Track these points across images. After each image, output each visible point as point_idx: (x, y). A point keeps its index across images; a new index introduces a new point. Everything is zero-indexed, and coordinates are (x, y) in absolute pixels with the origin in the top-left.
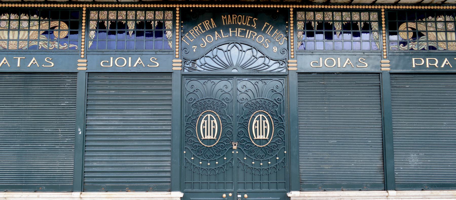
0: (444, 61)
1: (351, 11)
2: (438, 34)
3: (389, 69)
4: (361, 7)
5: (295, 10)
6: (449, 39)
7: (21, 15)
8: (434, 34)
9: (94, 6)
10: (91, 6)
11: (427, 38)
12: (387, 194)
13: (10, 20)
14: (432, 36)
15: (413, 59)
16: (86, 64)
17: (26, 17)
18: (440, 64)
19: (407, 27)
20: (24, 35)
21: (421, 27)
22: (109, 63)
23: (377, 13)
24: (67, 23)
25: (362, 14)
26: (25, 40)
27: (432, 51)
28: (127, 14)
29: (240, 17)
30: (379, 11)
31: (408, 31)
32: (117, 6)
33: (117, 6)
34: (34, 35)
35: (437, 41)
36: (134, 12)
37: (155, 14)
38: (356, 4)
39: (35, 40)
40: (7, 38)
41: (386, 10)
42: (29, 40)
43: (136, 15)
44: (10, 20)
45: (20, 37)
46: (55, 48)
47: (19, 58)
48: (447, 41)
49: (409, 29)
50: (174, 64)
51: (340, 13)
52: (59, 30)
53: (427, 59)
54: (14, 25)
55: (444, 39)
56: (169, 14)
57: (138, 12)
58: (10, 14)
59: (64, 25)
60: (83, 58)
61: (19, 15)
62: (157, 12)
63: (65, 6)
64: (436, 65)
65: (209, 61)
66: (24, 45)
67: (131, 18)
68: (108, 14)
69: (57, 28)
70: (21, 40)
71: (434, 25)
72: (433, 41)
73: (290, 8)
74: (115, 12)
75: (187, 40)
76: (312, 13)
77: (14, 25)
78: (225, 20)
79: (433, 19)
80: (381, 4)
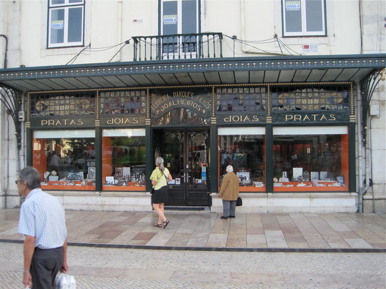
0: (305, 116)
3: (215, 123)
4: (255, 84)
5: (216, 88)
6: (309, 103)
7: (314, 89)
9: (103, 89)
10: (101, 89)
13: (60, 99)
14: (52, 108)
15: (286, 116)
17: (317, 91)
18: (55, 123)
19: (40, 103)
21: (47, 103)
23: (265, 88)
28: (120, 94)
29: (184, 93)
30: (146, 90)
31: (40, 106)
32: (115, 89)
33: (115, 89)
34: (72, 107)
35: (55, 111)
37: (135, 93)
38: (281, 82)
39: (73, 110)
40: (59, 109)
42: (320, 104)
43: (125, 94)
44: (60, 99)
45: (66, 108)
46: (83, 114)
47: (65, 120)
49: (41, 105)
50: (146, 122)
51: (242, 89)
52: (85, 105)
53: (295, 116)
56: (144, 93)
57: (126, 92)
58: (60, 96)
60: (98, 119)
61: (313, 89)
64: (300, 119)
66: (67, 113)
72: (53, 111)
73: (212, 86)
74: (114, 93)
76: (226, 89)
78: (175, 95)
79: (300, 91)
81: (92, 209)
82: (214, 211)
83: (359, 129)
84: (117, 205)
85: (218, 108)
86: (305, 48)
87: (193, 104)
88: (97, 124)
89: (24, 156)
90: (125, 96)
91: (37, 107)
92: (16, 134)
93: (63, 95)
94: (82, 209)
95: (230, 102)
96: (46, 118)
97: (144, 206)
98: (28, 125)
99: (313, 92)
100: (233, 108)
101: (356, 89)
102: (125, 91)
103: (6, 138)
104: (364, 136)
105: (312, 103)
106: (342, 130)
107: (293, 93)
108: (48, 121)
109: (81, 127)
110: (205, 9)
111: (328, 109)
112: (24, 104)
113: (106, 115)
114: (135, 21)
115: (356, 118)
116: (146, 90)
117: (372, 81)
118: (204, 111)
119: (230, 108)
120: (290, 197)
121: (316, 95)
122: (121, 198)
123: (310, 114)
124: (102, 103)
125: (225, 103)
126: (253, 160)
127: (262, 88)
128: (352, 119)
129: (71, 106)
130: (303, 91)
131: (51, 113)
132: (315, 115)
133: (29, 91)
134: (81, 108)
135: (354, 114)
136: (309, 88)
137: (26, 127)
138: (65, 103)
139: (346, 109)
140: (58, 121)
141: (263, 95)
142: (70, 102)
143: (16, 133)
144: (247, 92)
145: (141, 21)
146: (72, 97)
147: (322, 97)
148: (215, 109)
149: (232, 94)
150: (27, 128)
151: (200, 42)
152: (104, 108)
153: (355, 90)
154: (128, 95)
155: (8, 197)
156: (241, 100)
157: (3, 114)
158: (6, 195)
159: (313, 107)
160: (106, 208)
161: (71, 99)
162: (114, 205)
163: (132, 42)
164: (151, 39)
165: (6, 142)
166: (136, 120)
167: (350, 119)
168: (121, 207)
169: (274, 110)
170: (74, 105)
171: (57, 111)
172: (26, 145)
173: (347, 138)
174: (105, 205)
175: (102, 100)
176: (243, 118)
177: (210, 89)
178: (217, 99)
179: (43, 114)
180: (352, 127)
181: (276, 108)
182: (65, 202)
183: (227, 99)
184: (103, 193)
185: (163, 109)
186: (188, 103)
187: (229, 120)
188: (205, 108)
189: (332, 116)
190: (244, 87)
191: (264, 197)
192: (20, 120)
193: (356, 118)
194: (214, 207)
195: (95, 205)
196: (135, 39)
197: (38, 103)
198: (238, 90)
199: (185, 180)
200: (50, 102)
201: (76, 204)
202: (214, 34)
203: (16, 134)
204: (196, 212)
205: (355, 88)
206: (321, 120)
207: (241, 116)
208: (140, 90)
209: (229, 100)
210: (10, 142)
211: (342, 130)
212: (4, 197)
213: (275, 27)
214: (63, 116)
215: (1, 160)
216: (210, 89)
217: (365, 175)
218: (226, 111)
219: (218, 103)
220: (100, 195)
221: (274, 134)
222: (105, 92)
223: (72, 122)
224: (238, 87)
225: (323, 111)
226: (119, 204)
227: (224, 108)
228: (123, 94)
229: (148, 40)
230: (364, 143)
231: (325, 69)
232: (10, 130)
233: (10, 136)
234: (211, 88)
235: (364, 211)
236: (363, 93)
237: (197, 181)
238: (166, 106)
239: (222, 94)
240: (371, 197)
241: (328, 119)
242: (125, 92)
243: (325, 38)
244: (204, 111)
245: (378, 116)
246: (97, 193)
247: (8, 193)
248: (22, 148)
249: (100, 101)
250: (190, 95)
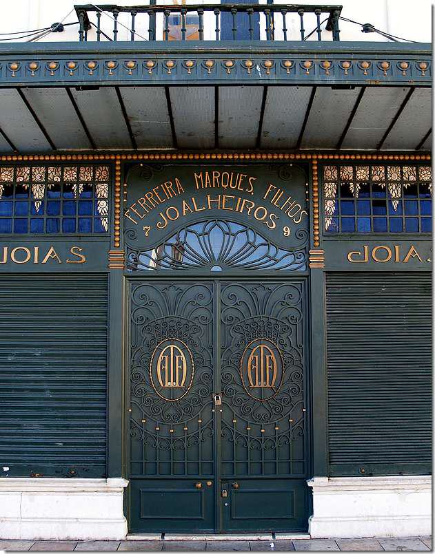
36: (43, 169)
43: (47, 174)
73: (312, 159)
74: (12, 169)
76: (350, 169)
152: (336, 212)
166: (79, 252)
176: (403, 254)
177: (305, 167)
190: (401, 164)
196: (81, 11)
198: (386, 170)
207: (36, 249)
216: (305, 167)
223: (49, 255)
242: (402, 169)
249: (322, 191)
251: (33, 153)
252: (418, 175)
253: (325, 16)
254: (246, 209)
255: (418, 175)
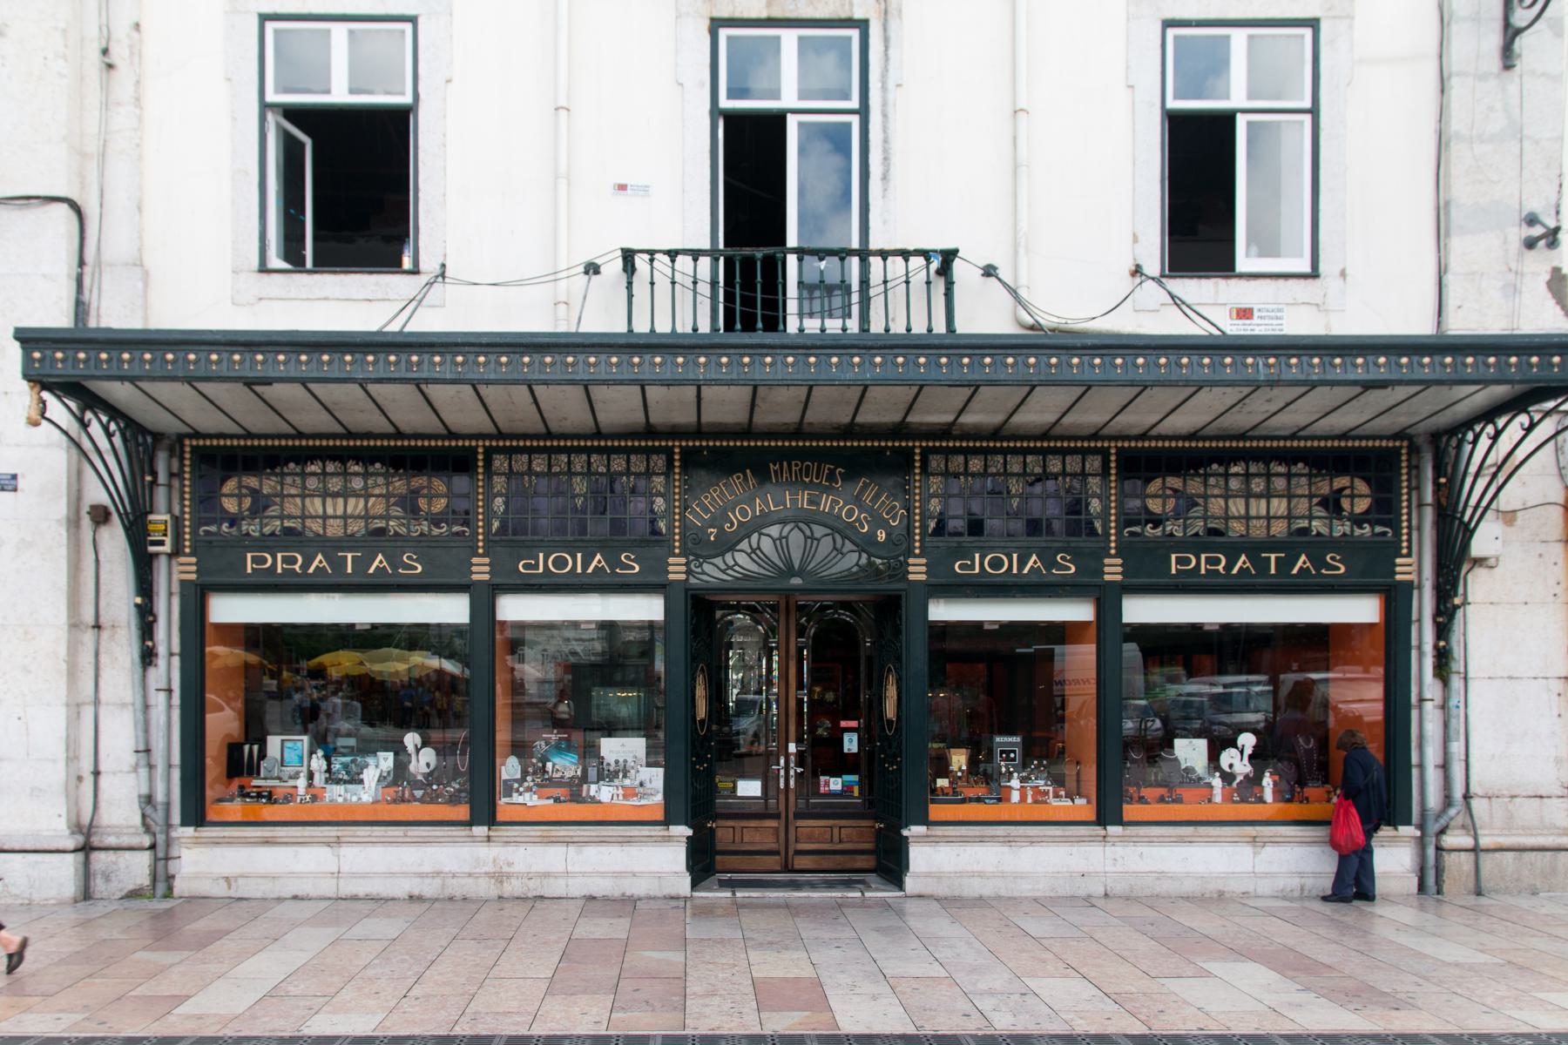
1: (549, 451)
2: (308, 500)
3: (487, 577)
8: (1222, 502)
11: (1206, 510)
12: (1103, 833)
13: (324, 473)
14: (1216, 506)
15: (1173, 556)
16: (684, 568)
17: (1282, 469)
18: (306, 566)
20: (356, 506)
22: (536, 566)
24: (1367, 480)
25: (1068, 459)
26: (359, 517)
27: (1212, 539)
28: (569, 462)
30: (1104, 453)
31: (1165, 497)
34: (1302, 506)
35: (304, 517)
36: (584, 457)
37: (628, 461)
39: (381, 517)
40: (321, 512)
41: (1120, 451)
42: (367, 517)
43: (589, 463)
44: (324, 473)
45: (349, 511)
46: (422, 534)
47: (349, 556)
48: (1247, 517)
49: (1169, 492)
52: (430, 498)
53: (1203, 556)
54: (1258, 485)
55: (1243, 512)
57: (594, 457)
59: (1361, 487)
60: (679, 556)
61: (1267, 465)
62: (633, 458)
63: (1336, 444)
64: (1220, 568)
65: (742, 559)
66: (356, 527)
67: (579, 469)
68: (530, 462)
69: (1348, 492)
70: (352, 517)
71: (1222, 483)
74: (545, 456)
75: (693, 512)
76: (961, 459)
77: (1258, 485)
79: (1221, 470)
80: (1110, 438)
81: (458, 893)
82: (916, 891)
83: (1424, 604)
84: (555, 875)
85: (932, 525)
86: (1239, 317)
87: (841, 509)
88: (481, 570)
89: (1421, 700)
90: (589, 473)
91: (224, 500)
92: (137, 605)
93: (341, 456)
94: (416, 892)
95: (976, 507)
96: (269, 543)
97: (659, 876)
98: (188, 568)
99: (345, 474)
100: (988, 523)
101: (1417, 467)
102: (589, 451)
103: (89, 618)
104: (1443, 630)
105: (340, 512)
106: (1362, 610)
107: (1199, 475)
108: (275, 559)
109: (633, 580)
110: (885, 159)
111: (1319, 534)
112: (169, 486)
113: (514, 538)
114: (622, 187)
115: (1416, 566)
116: (669, 452)
117: (1484, 442)
118: (881, 536)
119: (976, 527)
120: (1181, 840)
121: (357, 484)
122: (572, 849)
123: (1255, 549)
124: (499, 494)
125: (956, 508)
126: (408, 704)
127: (1090, 459)
128: (1404, 570)
129: (372, 500)
130: (1234, 469)
131: (287, 524)
132: (1273, 556)
133: (190, 436)
134: (413, 511)
135: (1409, 555)
136: (1256, 459)
137: (176, 577)
138: (346, 487)
139: (1384, 534)
140: (320, 557)
141: (658, 481)
142: (366, 488)
143: (139, 600)
144: (1038, 470)
145: (645, 189)
146: (378, 465)
147: (1299, 492)
148: (924, 527)
149: (985, 474)
150: (183, 583)
151: (865, 283)
153: (1415, 468)
154: (602, 469)
155: (95, 855)
156: (1015, 496)
157: (74, 523)
158: (86, 849)
159: (1268, 527)
160: (513, 887)
161: (372, 474)
162: (546, 875)
163: (613, 267)
164: (695, 260)
165: (89, 637)
167: (1398, 569)
168: (571, 881)
169: (1132, 534)
170: (387, 496)
171: (312, 517)
172: (176, 648)
173: (1093, 631)
174: (509, 876)
175: (499, 483)
176: (1022, 562)
178: (934, 496)
179: (252, 528)
180: (1396, 600)
181: (1137, 529)
182: (345, 869)
183: (967, 492)
184: (207, 832)
185: (732, 524)
186: (825, 503)
187: (972, 567)
188: (884, 524)
189: (1333, 558)
191: (1091, 839)
192: (152, 549)
193: (1416, 566)
194: (917, 876)
195: (470, 875)
196: (628, 256)
197: (230, 486)
199: (782, 781)
200: (282, 484)
201: (392, 875)
202: (905, 254)
203: (137, 605)
204: (851, 895)
205: (1414, 462)
206: (1295, 571)
207: (1015, 556)
208: (648, 452)
209: (974, 494)
210: (105, 635)
211: (1362, 610)
212: (80, 856)
213: (1135, 239)
214: (339, 540)
215: (67, 705)
217: (148, 751)
218: (960, 534)
219: (935, 505)
220: (489, 839)
221: (1125, 620)
222: (510, 452)
224: (1005, 452)
225: (1299, 541)
226: (561, 868)
227: (952, 524)
228: (579, 462)
229: (684, 262)
230: (1443, 660)
231: (44, 403)
232: (103, 588)
233: (102, 612)
234: (909, 452)
235: (1445, 888)
236: (1443, 480)
237: (827, 784)
238: (744, 513)
239: (946, 474)
240: (1467, 841)
241: (1318, 570)
243: (1310, 281)
244: (881, 536)
245: (1492, 562)
246: (480, 830)
247: (95, 841)
248: (162, 661)
250: (831, 477)
251: (525, 436)
252: (1044, 466)
253: (936, 264)
254: (832, 508)
255: (1044, 466)
